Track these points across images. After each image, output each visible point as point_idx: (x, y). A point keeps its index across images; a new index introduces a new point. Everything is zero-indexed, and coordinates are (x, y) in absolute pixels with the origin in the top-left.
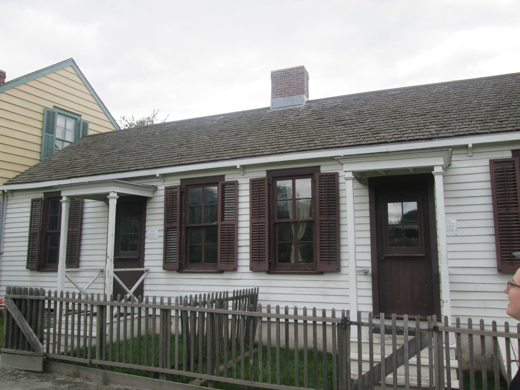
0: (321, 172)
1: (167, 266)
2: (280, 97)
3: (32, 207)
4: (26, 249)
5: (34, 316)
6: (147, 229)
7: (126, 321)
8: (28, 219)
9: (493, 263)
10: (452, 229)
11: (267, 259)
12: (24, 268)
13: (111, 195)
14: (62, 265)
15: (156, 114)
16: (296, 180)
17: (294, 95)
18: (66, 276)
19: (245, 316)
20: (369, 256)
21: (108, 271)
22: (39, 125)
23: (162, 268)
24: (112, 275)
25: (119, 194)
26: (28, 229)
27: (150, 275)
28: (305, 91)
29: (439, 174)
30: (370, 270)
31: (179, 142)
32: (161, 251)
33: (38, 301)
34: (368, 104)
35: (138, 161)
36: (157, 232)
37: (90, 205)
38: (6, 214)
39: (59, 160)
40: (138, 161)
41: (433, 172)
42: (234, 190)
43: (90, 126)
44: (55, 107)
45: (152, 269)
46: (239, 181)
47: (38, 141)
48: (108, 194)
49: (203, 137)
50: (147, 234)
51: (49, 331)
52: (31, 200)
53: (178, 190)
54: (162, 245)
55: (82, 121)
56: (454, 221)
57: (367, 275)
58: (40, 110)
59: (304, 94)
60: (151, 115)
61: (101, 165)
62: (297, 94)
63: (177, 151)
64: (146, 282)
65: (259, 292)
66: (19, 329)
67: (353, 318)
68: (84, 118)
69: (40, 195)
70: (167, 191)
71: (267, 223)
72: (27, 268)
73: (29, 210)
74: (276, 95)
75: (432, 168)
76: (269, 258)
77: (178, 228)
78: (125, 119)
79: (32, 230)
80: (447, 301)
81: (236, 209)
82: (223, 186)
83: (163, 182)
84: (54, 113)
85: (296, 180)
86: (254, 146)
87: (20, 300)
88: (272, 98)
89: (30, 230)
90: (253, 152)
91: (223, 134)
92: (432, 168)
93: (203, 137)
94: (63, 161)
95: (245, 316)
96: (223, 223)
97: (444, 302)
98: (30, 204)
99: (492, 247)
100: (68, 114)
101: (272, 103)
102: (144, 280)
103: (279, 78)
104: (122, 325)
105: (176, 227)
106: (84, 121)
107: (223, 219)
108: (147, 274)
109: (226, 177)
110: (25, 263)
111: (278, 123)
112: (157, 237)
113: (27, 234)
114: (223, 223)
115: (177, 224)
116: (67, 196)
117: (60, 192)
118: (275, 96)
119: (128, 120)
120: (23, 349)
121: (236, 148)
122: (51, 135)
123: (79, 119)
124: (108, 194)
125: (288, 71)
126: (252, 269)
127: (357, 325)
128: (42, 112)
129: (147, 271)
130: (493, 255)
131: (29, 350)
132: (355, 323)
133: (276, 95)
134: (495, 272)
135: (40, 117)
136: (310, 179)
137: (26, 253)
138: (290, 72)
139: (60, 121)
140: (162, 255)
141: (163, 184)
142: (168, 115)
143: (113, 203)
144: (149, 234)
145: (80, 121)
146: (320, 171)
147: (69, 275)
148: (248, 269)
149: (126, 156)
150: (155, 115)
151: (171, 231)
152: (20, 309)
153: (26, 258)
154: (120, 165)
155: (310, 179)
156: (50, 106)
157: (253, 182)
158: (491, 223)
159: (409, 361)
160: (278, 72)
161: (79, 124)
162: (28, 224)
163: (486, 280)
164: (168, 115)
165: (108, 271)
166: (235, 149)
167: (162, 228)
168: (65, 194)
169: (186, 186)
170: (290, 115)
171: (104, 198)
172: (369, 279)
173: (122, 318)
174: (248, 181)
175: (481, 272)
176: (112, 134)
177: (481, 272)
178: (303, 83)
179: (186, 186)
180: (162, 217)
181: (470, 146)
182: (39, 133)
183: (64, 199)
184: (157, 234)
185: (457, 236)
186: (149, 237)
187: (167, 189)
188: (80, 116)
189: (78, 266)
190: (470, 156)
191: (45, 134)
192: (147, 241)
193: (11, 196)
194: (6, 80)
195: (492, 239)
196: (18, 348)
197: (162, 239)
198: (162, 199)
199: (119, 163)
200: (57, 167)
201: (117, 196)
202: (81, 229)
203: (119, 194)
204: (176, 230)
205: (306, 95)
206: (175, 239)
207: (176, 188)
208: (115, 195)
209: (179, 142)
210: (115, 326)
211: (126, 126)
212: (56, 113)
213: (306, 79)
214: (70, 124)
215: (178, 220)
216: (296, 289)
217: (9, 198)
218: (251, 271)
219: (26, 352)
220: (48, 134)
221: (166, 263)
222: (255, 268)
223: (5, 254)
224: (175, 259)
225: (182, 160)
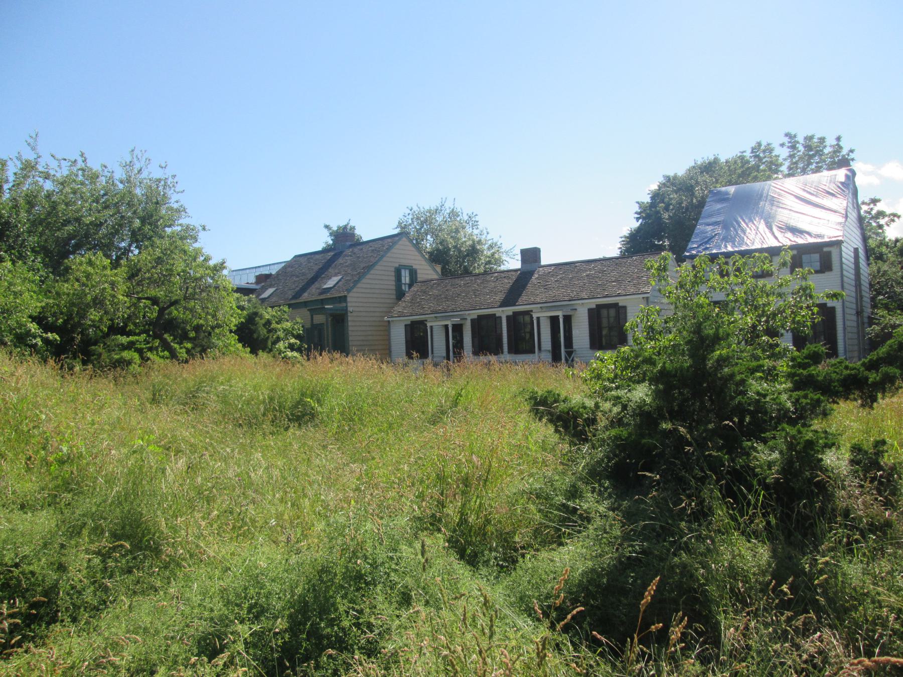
58: (393, 269)
100: (405, 267)
135: (393, 274)
156: (397, 265)
182: (394, 283)
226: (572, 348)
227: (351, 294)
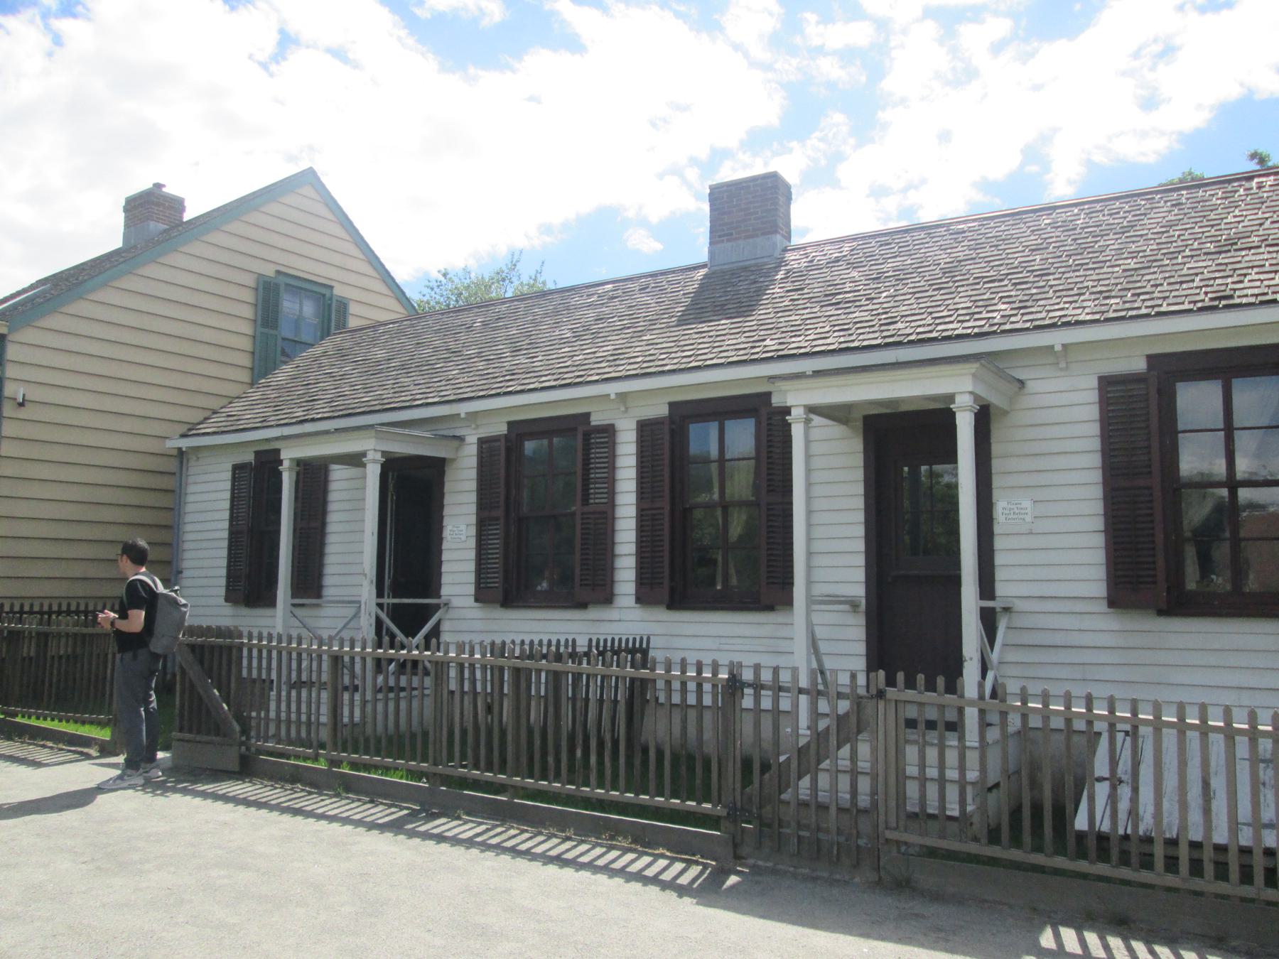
0: (774, 405)
1: (483, 594)
2: (728, 241)
3: (234, 479)
4: (224, 563)
5: (224, 673)
6: (445, 522)
7: (397, 700)
8: (227, 505)
9: (1100, 589)
10: (1024, 519)
11: (666, 581)
12: (221, 601)
13: (370, 455)
14: (285, 592)
15: (518, 261)
16: (1233, 380)
17: (757, 236)
18: (292, 612)
19: (568, 672)
20: (860, 575)
21: (366, 603)
22: (248, 312)
23: (472, 599)
24: (374, 609)
25: (384, 453)
26: (226, 525)
27: (452, 614)
28: (781, 225)
29: (963, 409)
30: (863, 601)
31: (514, 345)
32: (472, 566)
33: (230, 648)
34: (902, 254)
35: (430, 385)
36: (463, 527)
37: (339, 473)
38: (811, 553)
39: (287, 384)
40: (430, 385)
41: (952, 406)
42: (606, 442)
43: (353, 309)
44: (278, 272)
45: (455, 602)
46: (616, 426)
47: (246, 344)
48: (364, 454)
49: (563, 332)
50: (447, 533)
51: (259, 714)
52: (231, 466)
53: (502, 445)
54: (472, 554)
55: (334, 301)
56: (1027, 504)
57: (858, 612)
58: (250, 281)
59: (776, 232)
60: (507, 265)
61: (361, 395)
62: (763, 234)
63: (505, 364)
64: (445, 626)
65: (651, 646)
66: (200, 699)
67: (747, 675)
68: (339, 291)
69: (249, 457)
70: (482, 447)
71: (668, 508)
72: (226, 600)
73: (228, 485)
74: (720, 236)
75: (951, 398)
76: (672, 578)
77: (502, 521)
78: (448, 277)
79: (483, 588)
80: (971, 659)
81: (611, 481)
82: (587, 436)
83: (474, 429)
84: (277, 286)
85: (1233, 380)
86: (650, 352)
87: (202, 647)
88: (711, 243)
89: (231, 525)
90: (645, 365)
91: (601, 326)
92: (951, 398)
93: (563, 332)
94: (293, 387)
95: (568, 672)
96: (586, 509)
97: (966, 660)
98: (229, 475)
99: (1100, 556)
101: (712, 254)
102: (442, 622)
103: (725, 199)
104: (391, 705)
105: (497, 519)
106: (339, 299)
107: (585, 500)
108: (447, 611)
109: (592, 418)
110: (222, 591)
111: (713, 300)
112: (463, 538)
113: (225, 534)
114: (586, 509)
115: (500, 513)
116: (291, 459)
117: (277, 451)
118: (717, 239)
119: (454, 278)
120: (208, 733)
121: (616, 357)
122: (272, 332)
123: (328, 295)
124: (364, 454)
125: (744, 185)
126: (639, 600)
127: (754, 688)
128: (252, 284)
129: (446, 604)
130: (1100, 573)
131: (217, 734)
132: (750, 685)
133: (720, 236)
134: (1103, 606)
135: (249, 296)
136: (753, 420)
137: (224, 572)
138: (749, 187)
139: (289, 305)
140: (474, 574)
141: (474, 432)
142: (543, 263)
143: (373, 472)
144: (449, 532)
145: (331, 299)
146: (590, 422)
147: (298, 611)
148: (631, 601)
149: (409, 375)
150: (515, 265)
151: (490, 525)
152: (201, 662)
153: (223, 582)
154: (397, 395)
155: (753, 420)
156: (269, 271)
157: (642, 426)
158: (1098, 507)
159: (809, 739)
160: (723, 187)
161: (330, 306)
162: (226, 515)
163: (1088, 623)
164: (543, 263)
165: (366, 603)
166: (615, 360)
167: (473, 519)
168: (288, 455)
169: (517, 435)
170: (740, 281)
171: (355, 460)
172: (861, 620)
173: (391, 695)
174: (634, 426)
175: (1079, 607)
176: (391, 326)
177: (1079, 607)
178: (776, 210)
179: (517, 435)
180: (473, 497)
181: (1058, 348)
182: (247, 329)
183: (286, 464)
184: (464, 532)
185: (1032, 533)
186: (449, 537)
187: (481, 441)
188: (331, 287)
189: (319, 595)
190: (1061, 369)
191: (260, 329)
192: (445, 545)
193: (195, 458)
194: (187, 216)
195: (1100, 540)
196: (199, 732)
197: (472, 543)
198: (473, 462)
199: (397, 390)
200: (281, 399)
201: (382, 457)
202: (324, 524)
203: (384, 453)
204: (497, 524)
205: (783, 236)
206: (496, 543)
207: (663, 423)
208: (378, 456)
209: (514, 345)
210: (380, 707)
211: (438, 303)
212: (282, 288)
213: (782, 199)
214: (309, 309)
215: (502, 503)
216: (723, 641)
217: (192, 463)
218: (638, 605)
219: (214, 738)
220: (266, 330)
221: (480, 588)
222: (643, 599)
223: (186, 574)
224: (496, 581)
225: (510, 383)
226: (439, 596)
227: (28, 335)
